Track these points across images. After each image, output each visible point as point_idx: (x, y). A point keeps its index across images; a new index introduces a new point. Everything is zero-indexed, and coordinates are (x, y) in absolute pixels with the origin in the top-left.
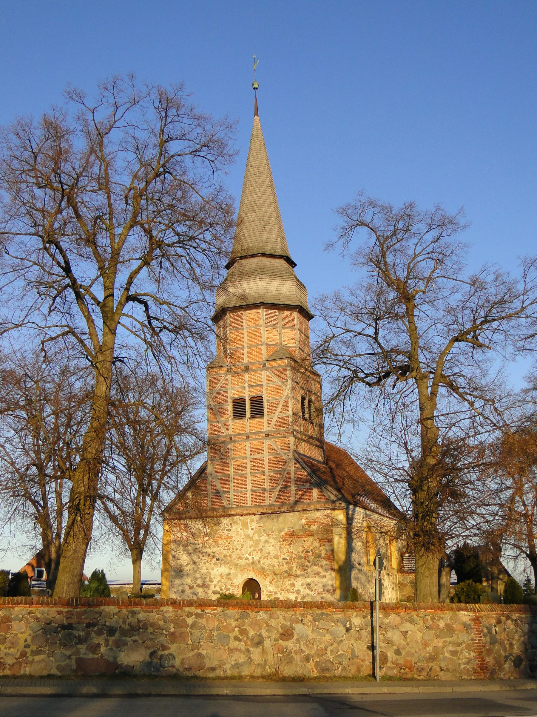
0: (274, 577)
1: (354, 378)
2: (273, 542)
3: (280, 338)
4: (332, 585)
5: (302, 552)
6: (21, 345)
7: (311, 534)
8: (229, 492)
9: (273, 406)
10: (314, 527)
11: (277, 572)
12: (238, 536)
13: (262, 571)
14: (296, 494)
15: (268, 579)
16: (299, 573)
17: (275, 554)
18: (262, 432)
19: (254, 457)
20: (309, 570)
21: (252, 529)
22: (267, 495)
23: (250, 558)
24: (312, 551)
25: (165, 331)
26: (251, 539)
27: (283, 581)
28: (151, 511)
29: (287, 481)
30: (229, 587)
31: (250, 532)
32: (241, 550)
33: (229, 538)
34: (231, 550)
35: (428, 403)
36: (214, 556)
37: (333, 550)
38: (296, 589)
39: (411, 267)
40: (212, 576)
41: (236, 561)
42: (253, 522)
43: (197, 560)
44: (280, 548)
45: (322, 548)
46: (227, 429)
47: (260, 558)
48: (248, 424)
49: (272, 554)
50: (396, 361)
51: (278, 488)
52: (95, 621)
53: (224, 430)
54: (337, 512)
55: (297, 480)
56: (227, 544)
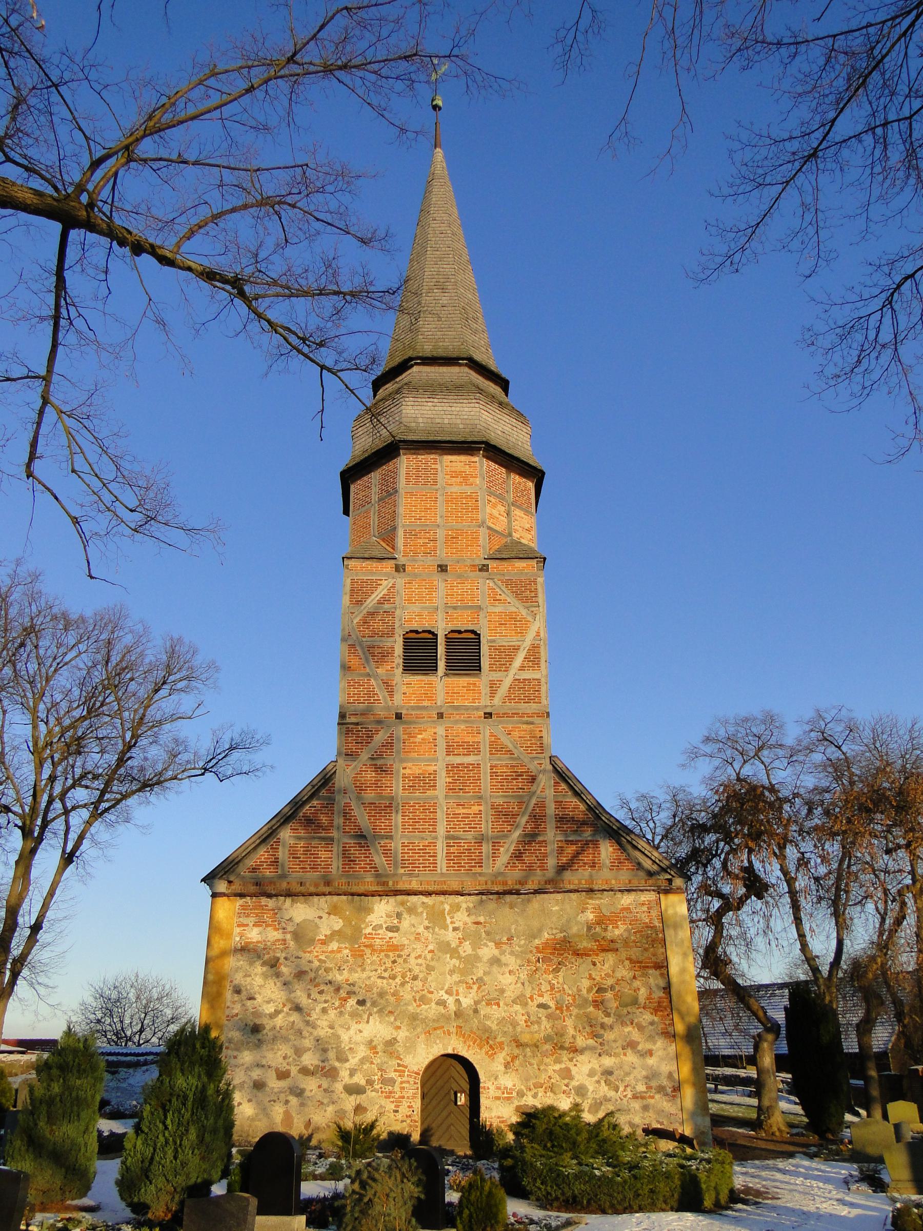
0: (516, 1051)
2: (512, 962)
3: (509, 522)
4: (670, 1075)
5: (589, 990)
7: (608, 947)
8: (391, 837)
9: (505, 656)
10: (618, 931)
11: (525, 1038)
12: (418, 946)
13: (486, 1039)
14: (561, 850)
15: (501, 1057)
16: (581, 1042)
17: (518, 993)
18: (477, 708)
19: (457, 760)
20: (609, 1036)
21: (455, 929)
22: (486, 848)
23: (451, 1001)
24: (612, 988)
26: (454, 953)
27: (541, 1063)
29: (537, 818)
30: (393, 1075)
31: (451, 936)
32: (425, 980)
33: (395, 948)
34: (398, 980)
36: (350, 993)
37: (668, 988)
38: (574, 1083)
40: (345, 1046)
41: (411, 1008)
42: (461, 914)
43: (304, 1001)
44: (531, 975)
45: (637, 983)
46: (391, 693)
47: (476, 1003)
48: (441, 685)
49: (510, 994)
51: (516, 834)
53: (382, 694)
54: (673, 898)
55: (561, 820)
56: (389, 965)
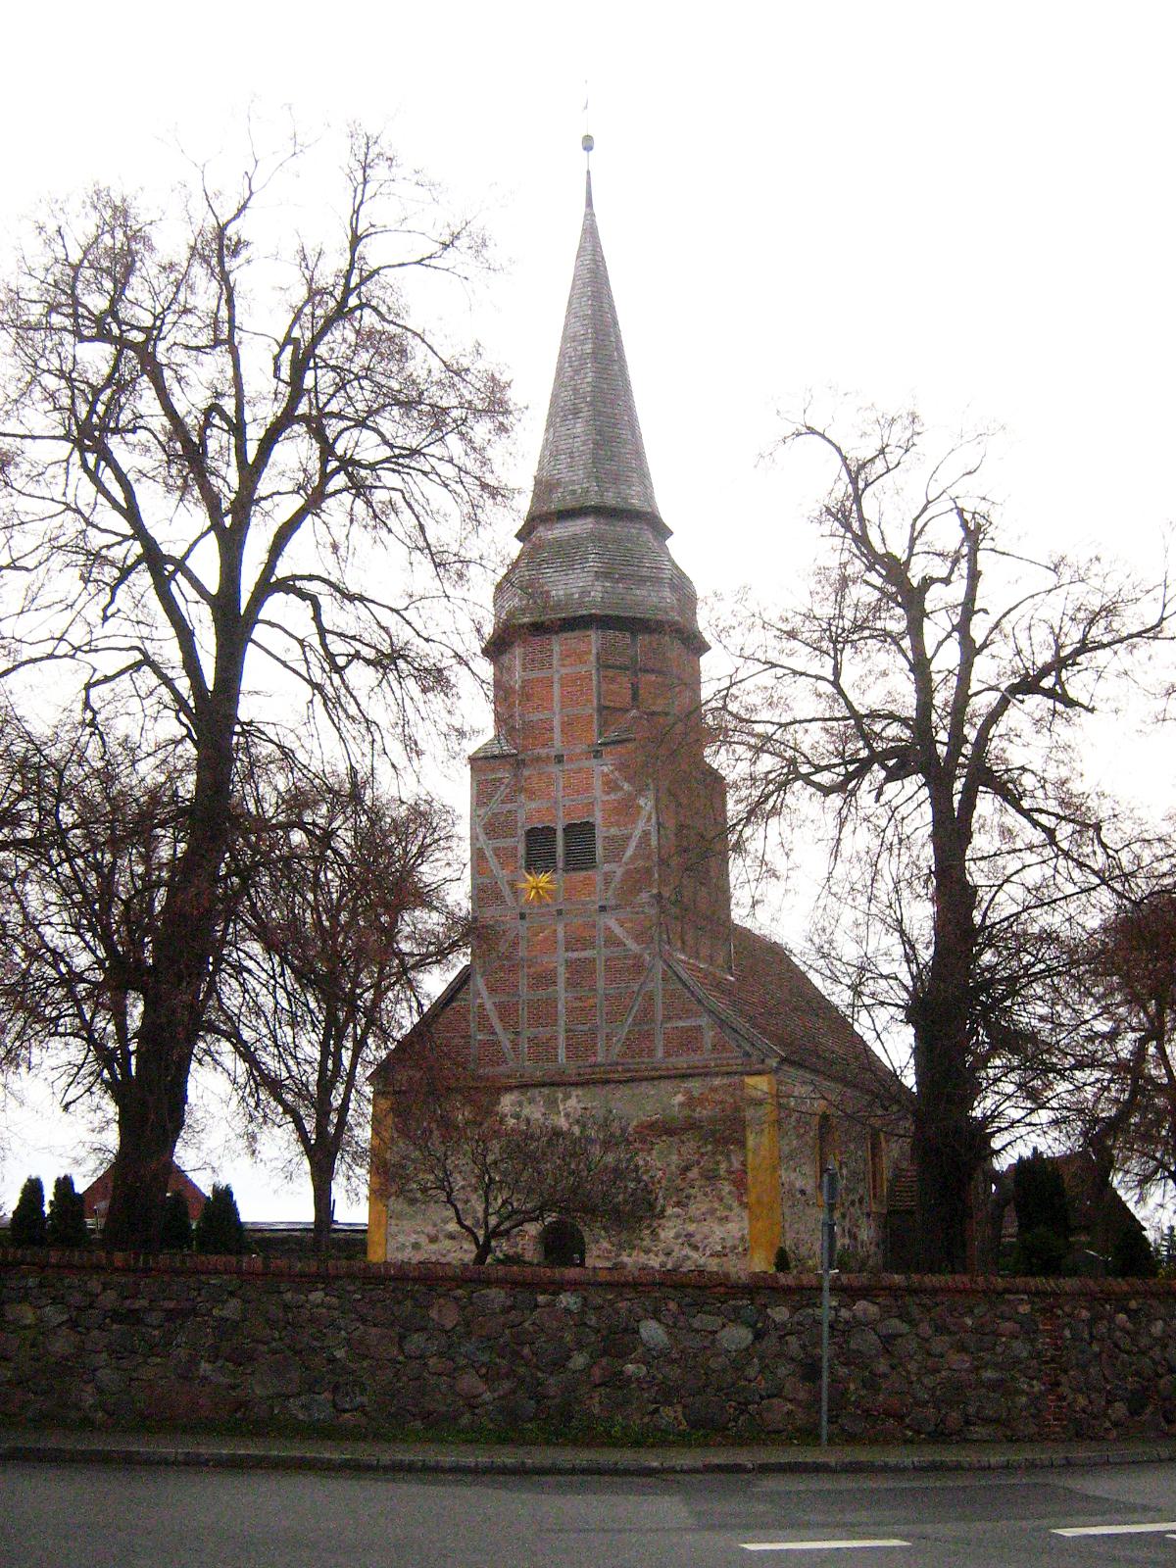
1: (792, 773)
6: (44, 703)
25: (357, 664)
28: (350, 1084)
35: (952, 833)
39: (918, 527)
50: (881, 738)
52: (188, 1305)
